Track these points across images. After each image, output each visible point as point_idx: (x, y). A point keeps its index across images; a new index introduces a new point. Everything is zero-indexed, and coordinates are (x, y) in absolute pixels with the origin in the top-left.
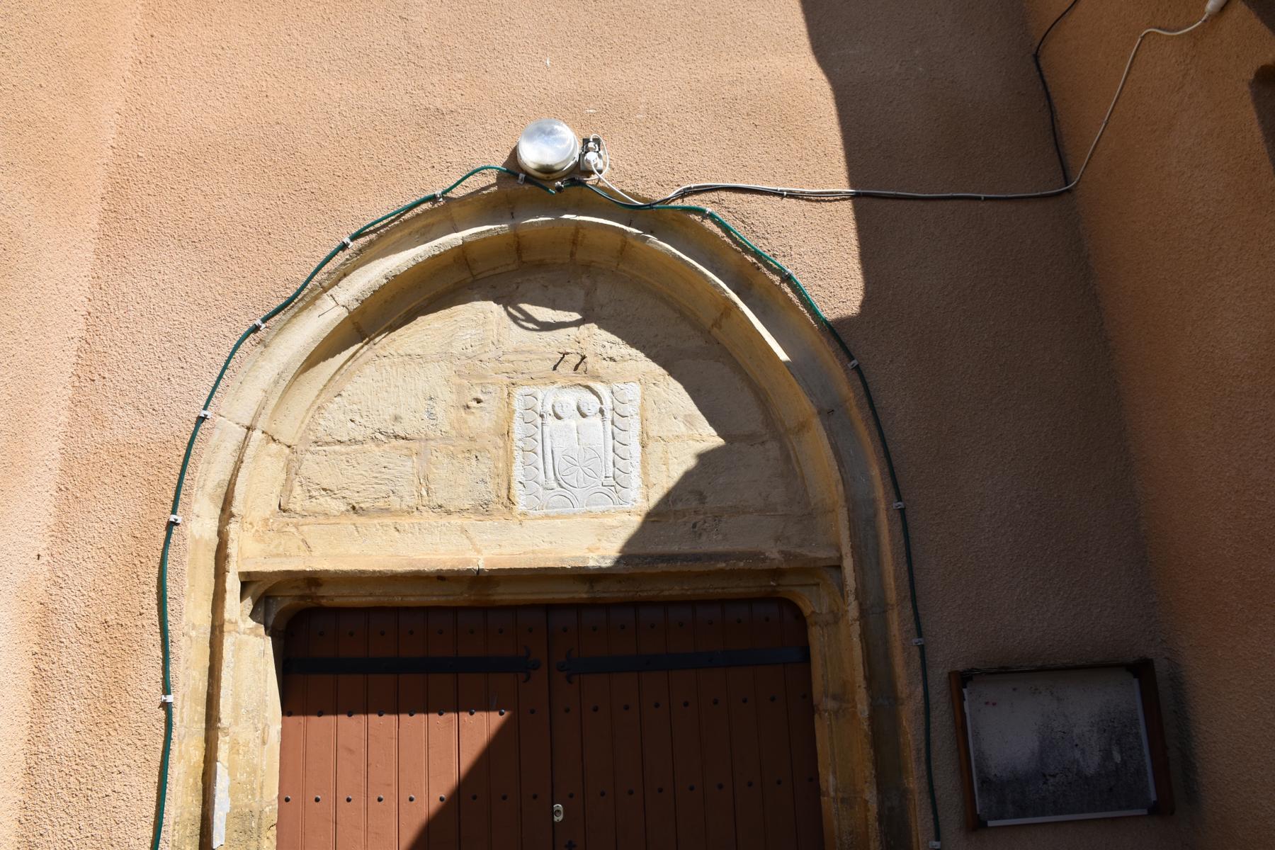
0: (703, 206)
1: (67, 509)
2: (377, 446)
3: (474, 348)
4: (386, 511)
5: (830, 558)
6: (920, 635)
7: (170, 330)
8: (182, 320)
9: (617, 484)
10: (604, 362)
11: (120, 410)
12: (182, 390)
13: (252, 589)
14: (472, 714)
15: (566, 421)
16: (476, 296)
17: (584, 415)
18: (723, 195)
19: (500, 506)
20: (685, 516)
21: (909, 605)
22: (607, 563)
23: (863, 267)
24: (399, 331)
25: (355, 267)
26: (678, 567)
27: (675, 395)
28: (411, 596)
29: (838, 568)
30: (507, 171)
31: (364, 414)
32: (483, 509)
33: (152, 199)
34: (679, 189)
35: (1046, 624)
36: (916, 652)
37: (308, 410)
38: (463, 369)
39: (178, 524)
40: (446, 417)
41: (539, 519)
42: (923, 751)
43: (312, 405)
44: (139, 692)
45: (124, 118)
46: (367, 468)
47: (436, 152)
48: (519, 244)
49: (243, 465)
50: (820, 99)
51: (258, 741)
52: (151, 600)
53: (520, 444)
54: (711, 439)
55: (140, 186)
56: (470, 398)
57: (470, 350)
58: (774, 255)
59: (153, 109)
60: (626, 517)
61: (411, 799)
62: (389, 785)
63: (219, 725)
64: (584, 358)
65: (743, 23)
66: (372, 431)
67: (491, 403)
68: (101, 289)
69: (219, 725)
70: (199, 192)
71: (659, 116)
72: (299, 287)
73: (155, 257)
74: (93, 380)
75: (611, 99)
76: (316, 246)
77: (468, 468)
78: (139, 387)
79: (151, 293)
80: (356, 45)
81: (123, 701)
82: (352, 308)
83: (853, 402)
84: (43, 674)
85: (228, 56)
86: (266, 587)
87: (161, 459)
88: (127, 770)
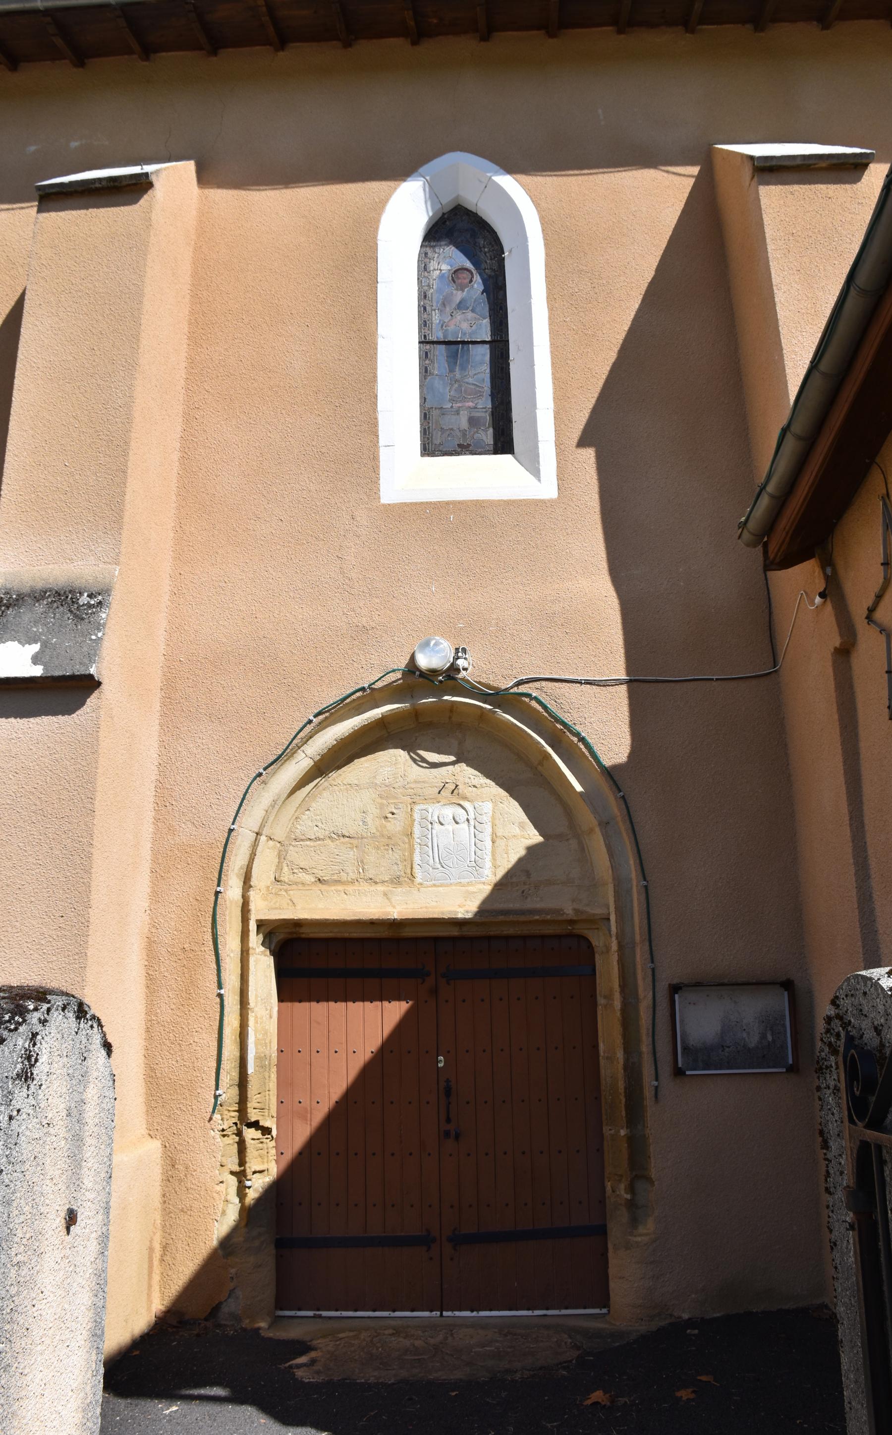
0: (530, 692)
1: (157, 883)
2: (332, 841)
3: (390, 780)
4: (338, 882)
5: (603, 914)
6: (652, 962)
7: (209, 775)
8: (216, 769)
9: (477, 865)
11: (183, 824)
13: (263, 929)
14: (390, 1002)
15: (446, 826)
16: (391, 746)
17: (457, 823)
18: (544, 683)
19: (406, 879)
20: (517, 886)
21: (647, 944)
22: (469, 916)
23: (631, 730)
24: (343, 769)
25: (316, 733)
26: (511, 918)
27: (514, 810)
28: (354, 933)
29: (609, 919)
30: (408, 671)
31: (324, 822)
32: (396, 881)
33: (191, 690)
34: (516, 680)
35: (732, 957)
36: (650, 973)
37: (290, 820)
38: (383, 793)
39: (221, 893)
40: (373, 824)
41: (429, 887)
42: (651, 1030)
43: (292, 817)
45: (169, 634)
46: (327, 856)
47: (364, 657)
48: (416, 712)
49: (256, 857)
50: (610, 611)
51: (268, 1016)
52: (209, 937)
53: (418, 841)
54: (534, 837)
56: (388, 812)
57: (387, 781)
58: (574, 724)
59: (186, 628)
60: (481, 886)
61: (354, 1052)
62: (342, 1044)
63: (249, 1006)
64: (457, 786)
65: (563, 553)
66: (329, 833)
67: (401, 815)
69: (249, 1006)
70: (219, 685)
71: (504, 628)
72: (284, 748)
75: (473, 616)
77: (387, 856)
78: (193, 810)
79: (195, 751)
80: (310, 578)
81: (196, 992)
82: (316, 760)
83: (619, 819)
84: (151, 977)
85: (229, 587)
86: (271, 928)
88: (201, 1030)
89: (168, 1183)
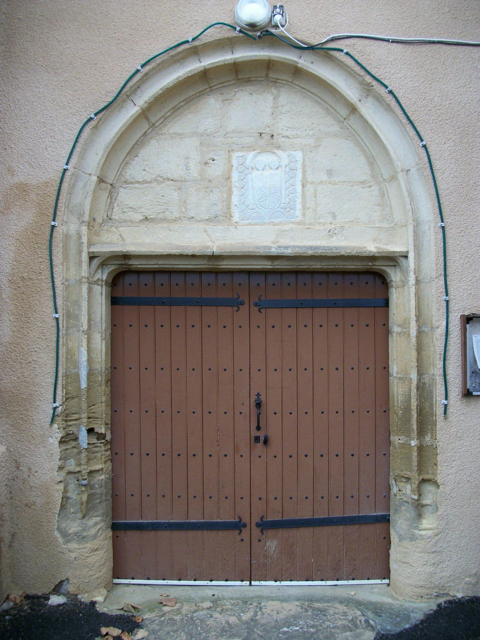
4: (164, 220)
8: (51, 115)
10: (283, 139)
12: (53, 154)
43: (122, 162)
44: (41, 312)
55: (22, 36)
66: (155, 176)
68: (5, 97)
70: (55, 39)
73: (33, 79)
74: (6, 149)
76: (122, 72)
87: (45, 192)
88: (39, 350)
89: (13, 482)
